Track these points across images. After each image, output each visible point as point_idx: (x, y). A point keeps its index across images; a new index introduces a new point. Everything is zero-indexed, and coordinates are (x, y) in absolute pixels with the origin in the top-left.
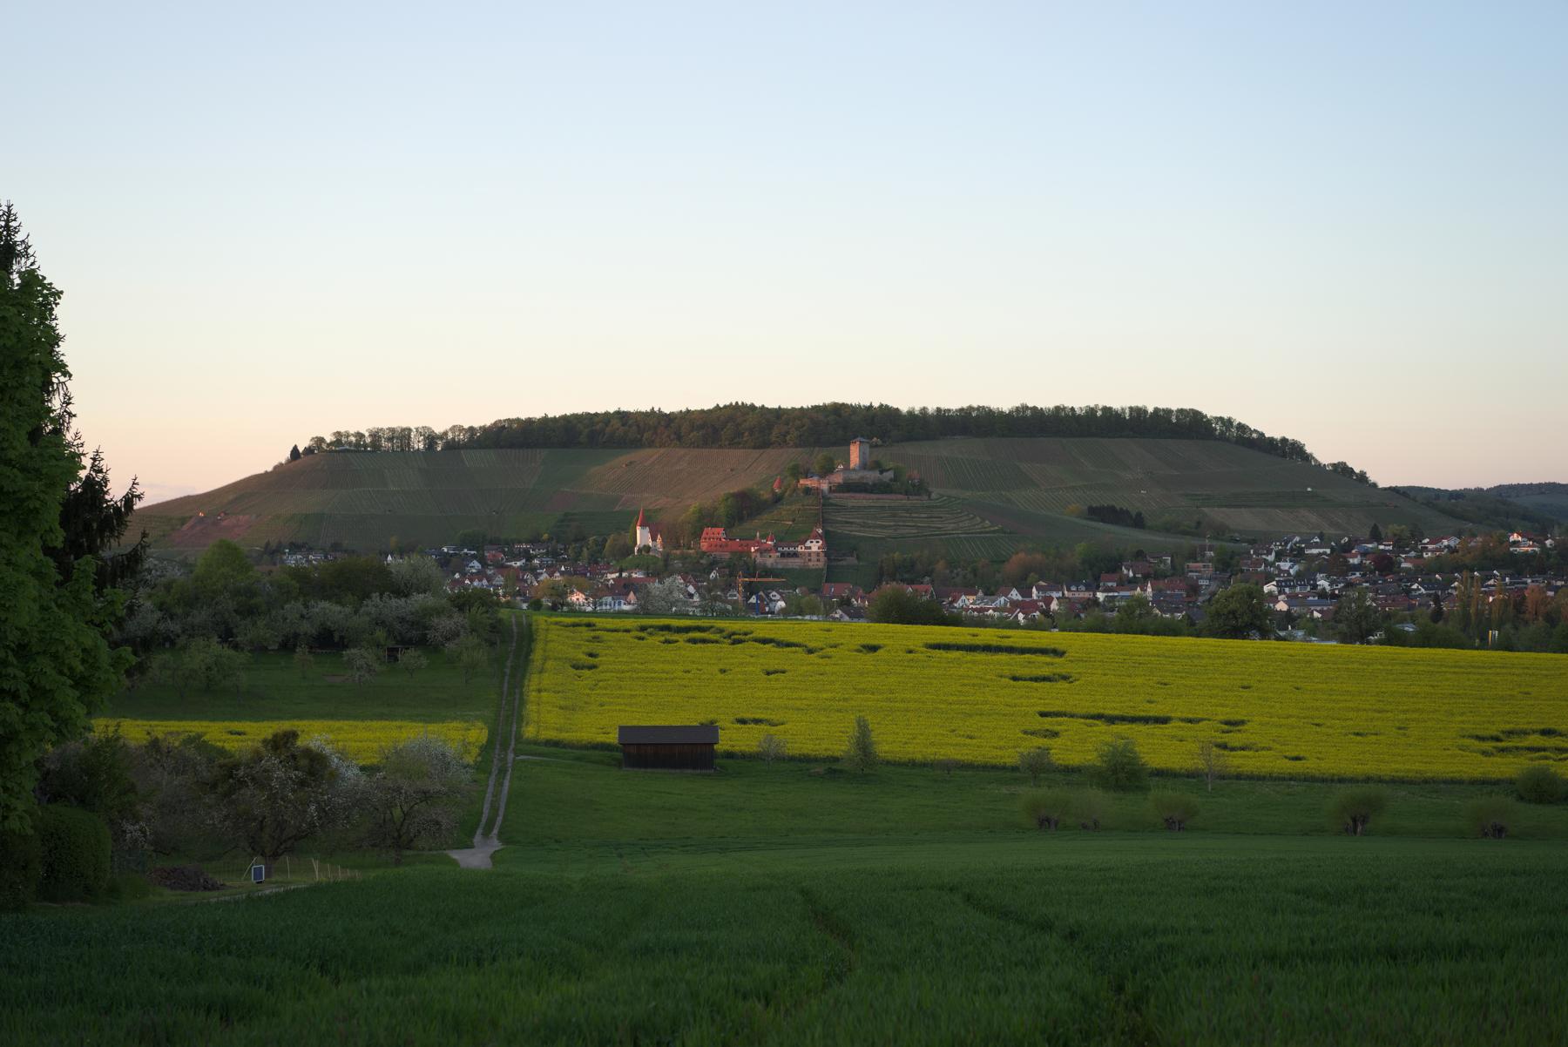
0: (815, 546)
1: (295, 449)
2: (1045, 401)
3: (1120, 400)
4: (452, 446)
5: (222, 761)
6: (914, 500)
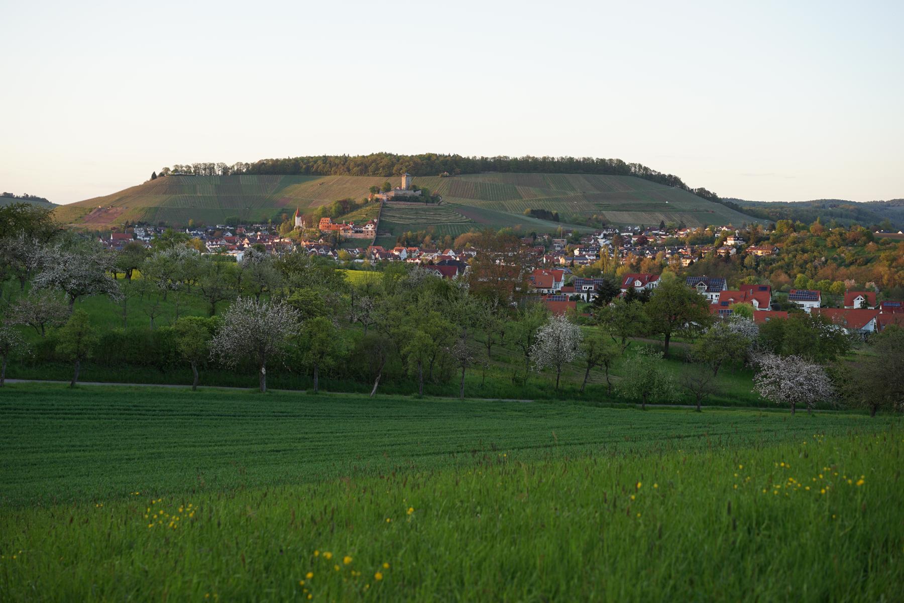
0: (370, 228)
1: (154, 175)
2: (539, 154)
3: (578, 155)
4: (238, 173)
5: (602, 254)
6: (430, 205)
